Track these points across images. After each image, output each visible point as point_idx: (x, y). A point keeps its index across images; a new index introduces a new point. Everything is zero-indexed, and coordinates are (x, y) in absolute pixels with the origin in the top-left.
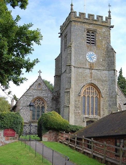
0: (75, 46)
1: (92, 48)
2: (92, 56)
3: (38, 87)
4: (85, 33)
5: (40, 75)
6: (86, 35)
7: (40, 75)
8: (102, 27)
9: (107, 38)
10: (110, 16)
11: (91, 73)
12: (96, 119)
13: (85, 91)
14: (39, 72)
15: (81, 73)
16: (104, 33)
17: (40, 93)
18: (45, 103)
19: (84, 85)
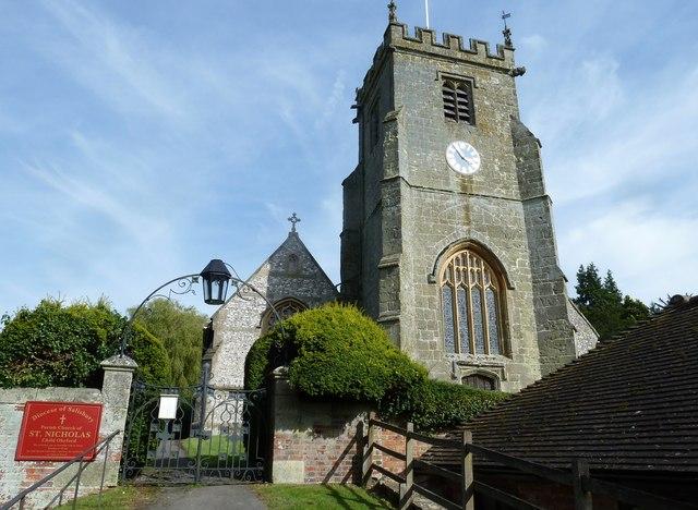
0: (409, 120)
1: (465, 131)
2: (464, 156)
3: (286, 266)
4: (439, 86)
5: (294, 229)
6: (440, 91)
7: (294, 229)
8: (489, 71)
9: (511, 100)
10: (508, 43)
11: (467, 208)
13: (450, 267)
14: (290, 219)
15: (434, 205)
16: (497, 88)
17: (295, 286)
19: (447, 248)
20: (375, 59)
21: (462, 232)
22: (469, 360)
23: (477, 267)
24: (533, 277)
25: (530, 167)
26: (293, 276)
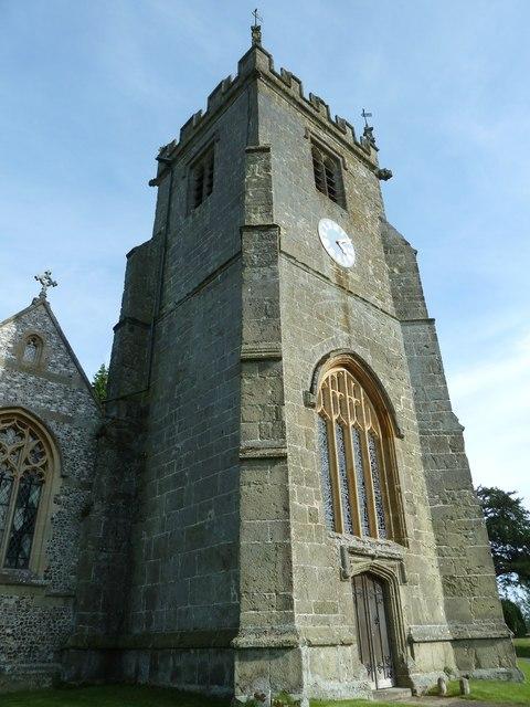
2: (336, 241)
5: (43, 295)
7: (43, 295)
12: (393, 563)
17: (31, 389)
18: (47, 456)
20: (210, 98)
21: (342, 340)
22: (361, 546)
23: (357, 398)
24: (420, 425)
25: (408, 282)
26: (30, 371)
